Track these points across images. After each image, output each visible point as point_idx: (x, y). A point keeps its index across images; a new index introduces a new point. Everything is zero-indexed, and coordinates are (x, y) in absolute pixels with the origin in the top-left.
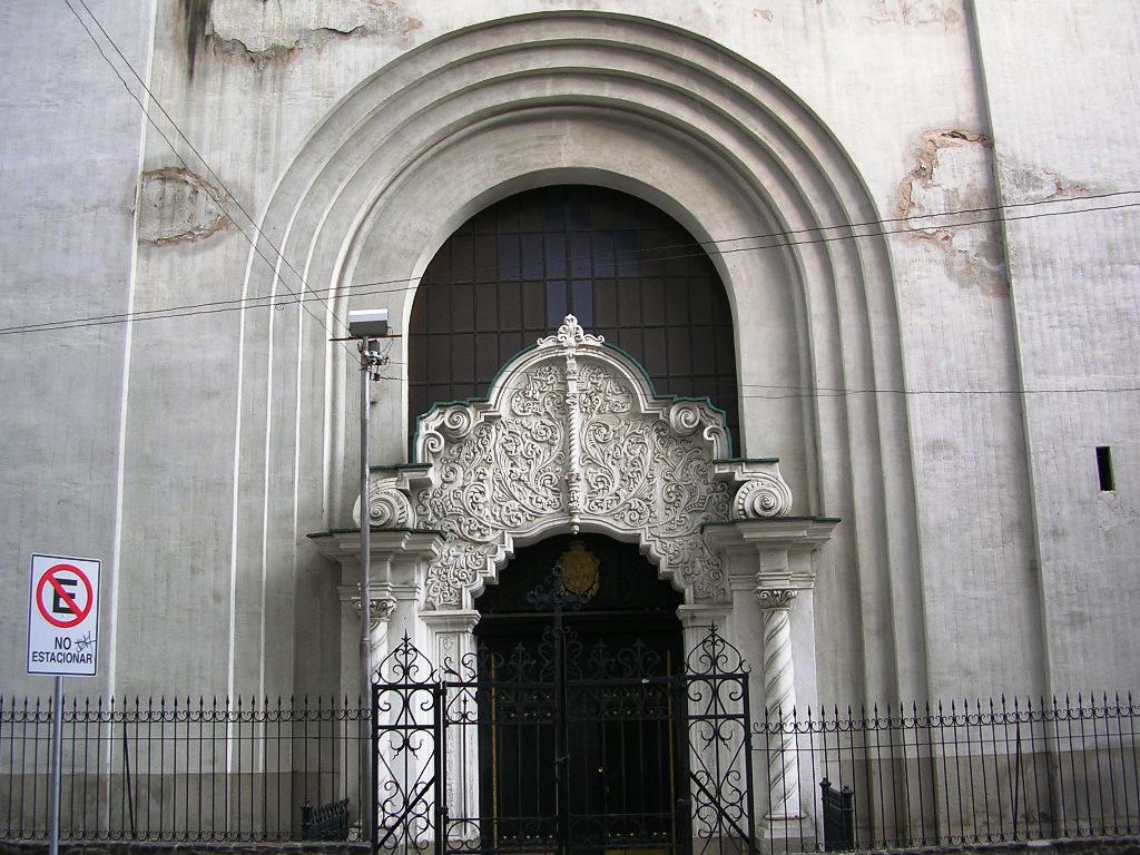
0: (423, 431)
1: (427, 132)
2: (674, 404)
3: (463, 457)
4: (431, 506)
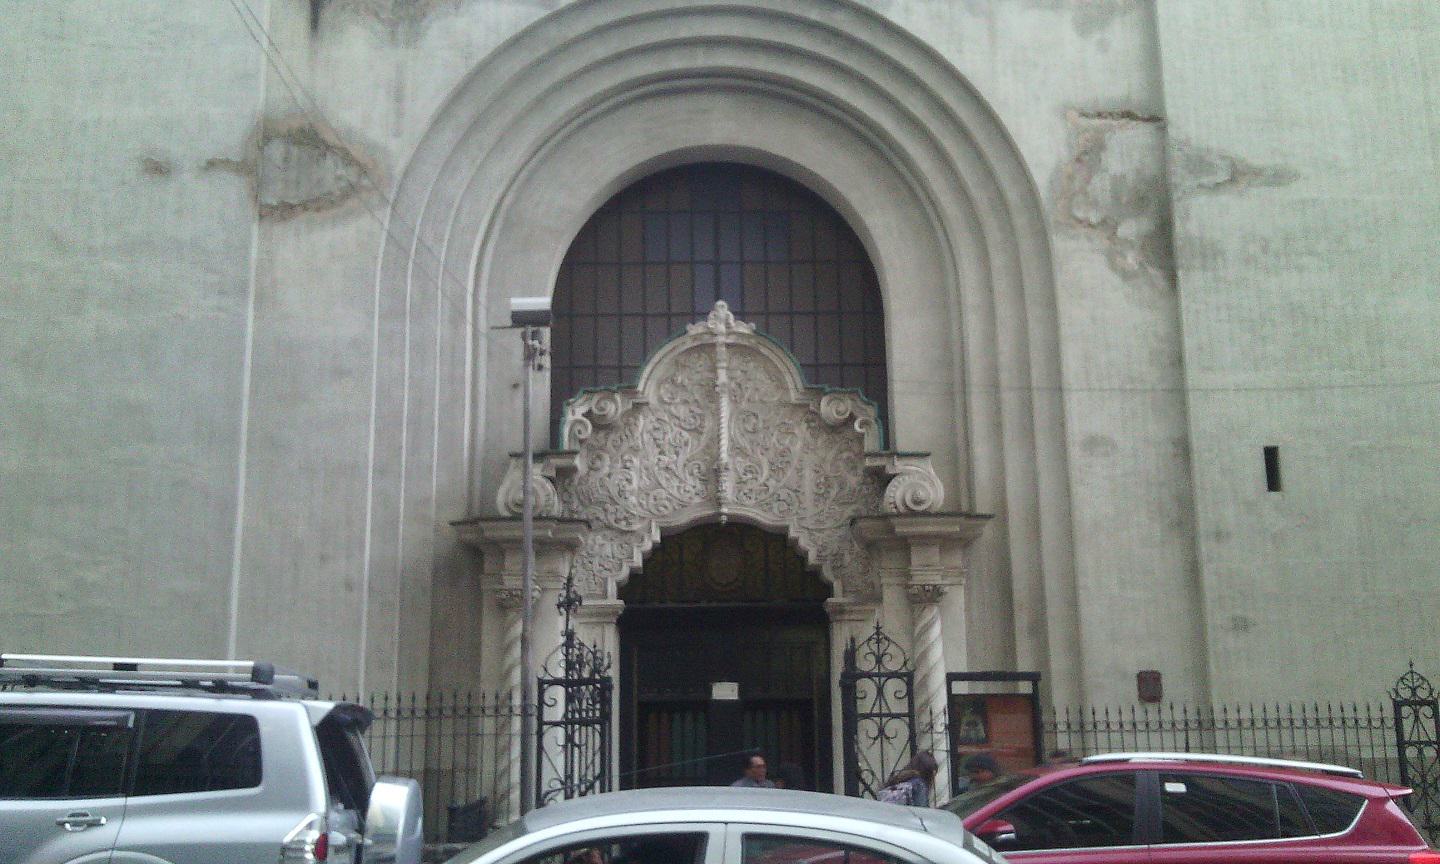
0: (569, 417)
1: (572, 100)
2: (826, 394)
3: (609, 444)
4: (577, 493)
